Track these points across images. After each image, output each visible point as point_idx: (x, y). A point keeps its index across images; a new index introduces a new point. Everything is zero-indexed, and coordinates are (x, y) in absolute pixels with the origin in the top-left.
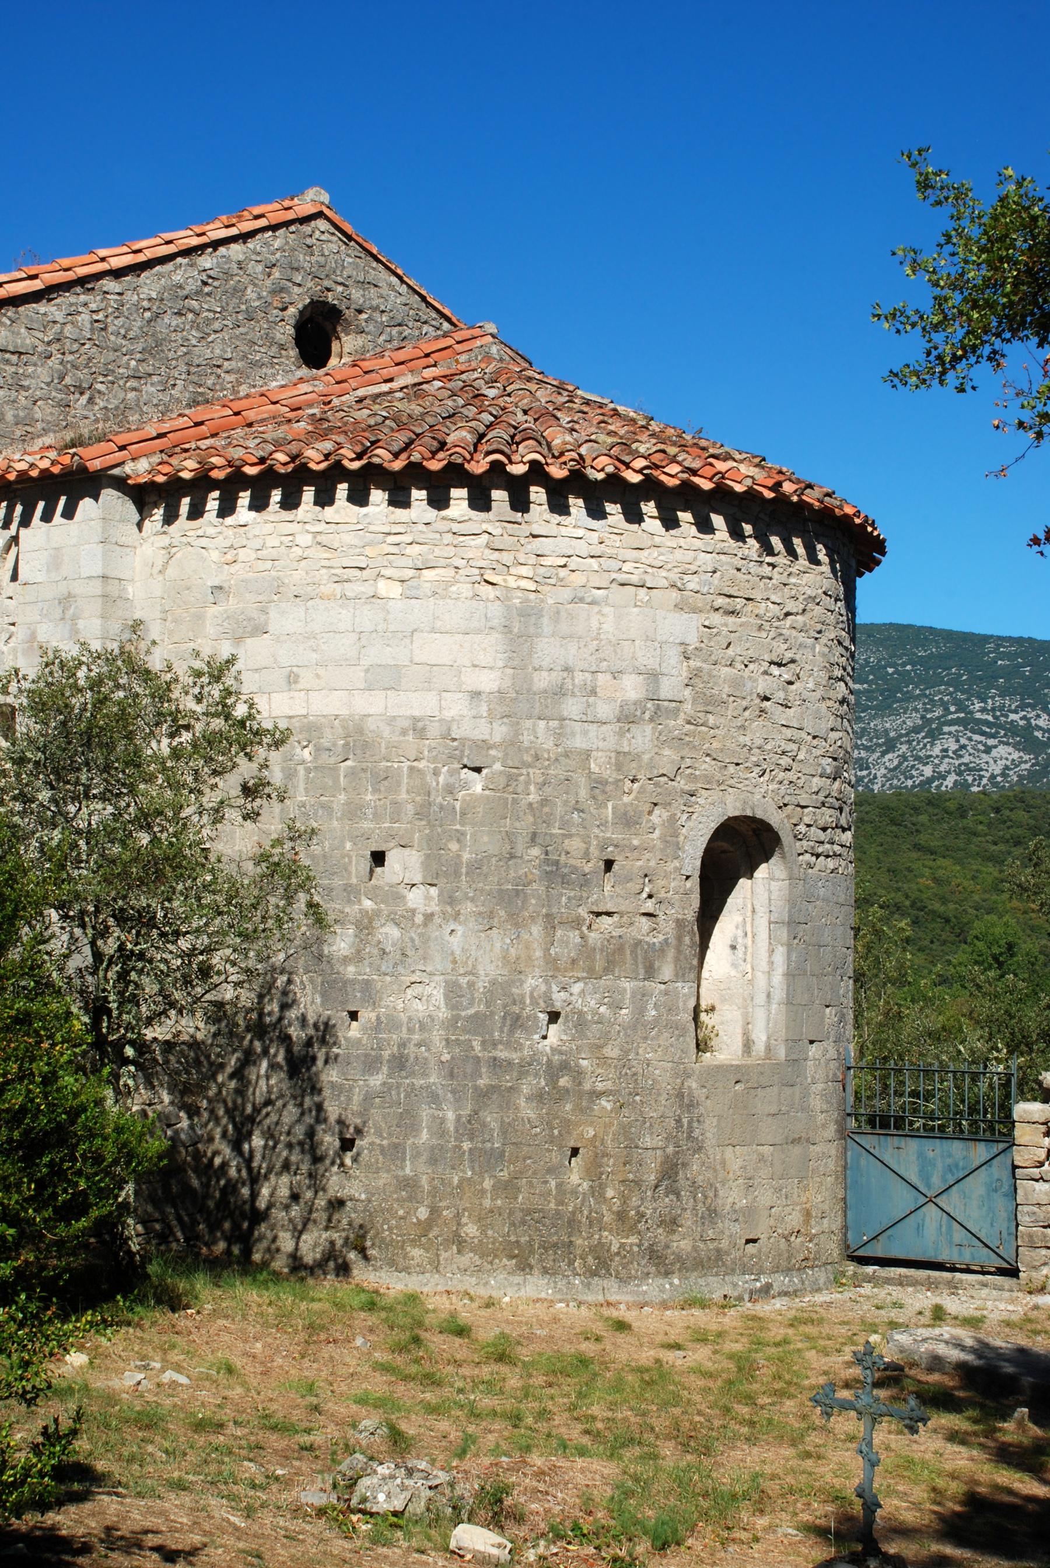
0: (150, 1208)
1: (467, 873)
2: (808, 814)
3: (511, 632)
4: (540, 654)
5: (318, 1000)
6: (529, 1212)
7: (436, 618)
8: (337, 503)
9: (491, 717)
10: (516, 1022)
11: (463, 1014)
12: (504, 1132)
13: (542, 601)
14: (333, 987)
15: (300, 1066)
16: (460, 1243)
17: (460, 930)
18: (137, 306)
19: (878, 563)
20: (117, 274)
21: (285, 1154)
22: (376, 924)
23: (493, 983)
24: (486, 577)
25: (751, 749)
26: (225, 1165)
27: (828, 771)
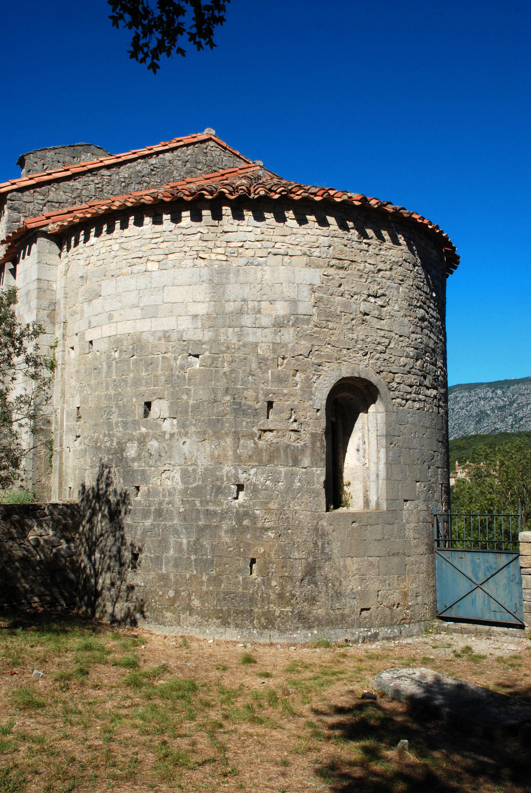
0: (42, 589)
1: (192, 411)
2: (398, 377)
3: (213, 283)
4: (229, 293)
5: (122, 481)
6: (227, 593)
7: (175, 278)
8: (130, 227)
9: (203, 327)
10: (219, 490)
11: (190, 486)
12: (213, 550)
13: (230, 265)
14: (128, 474)
15: (114, 516)
16: (190, 610)
17: (188, 441)
18: (118, 181)
19: (458, 257)
20: (108, 167)
21: (108, 561)
22: (147, 440)
23: (206, 469)
24: (200, 255)
25: (357, 341)
26: (85, 567)
27: (412, 354)
